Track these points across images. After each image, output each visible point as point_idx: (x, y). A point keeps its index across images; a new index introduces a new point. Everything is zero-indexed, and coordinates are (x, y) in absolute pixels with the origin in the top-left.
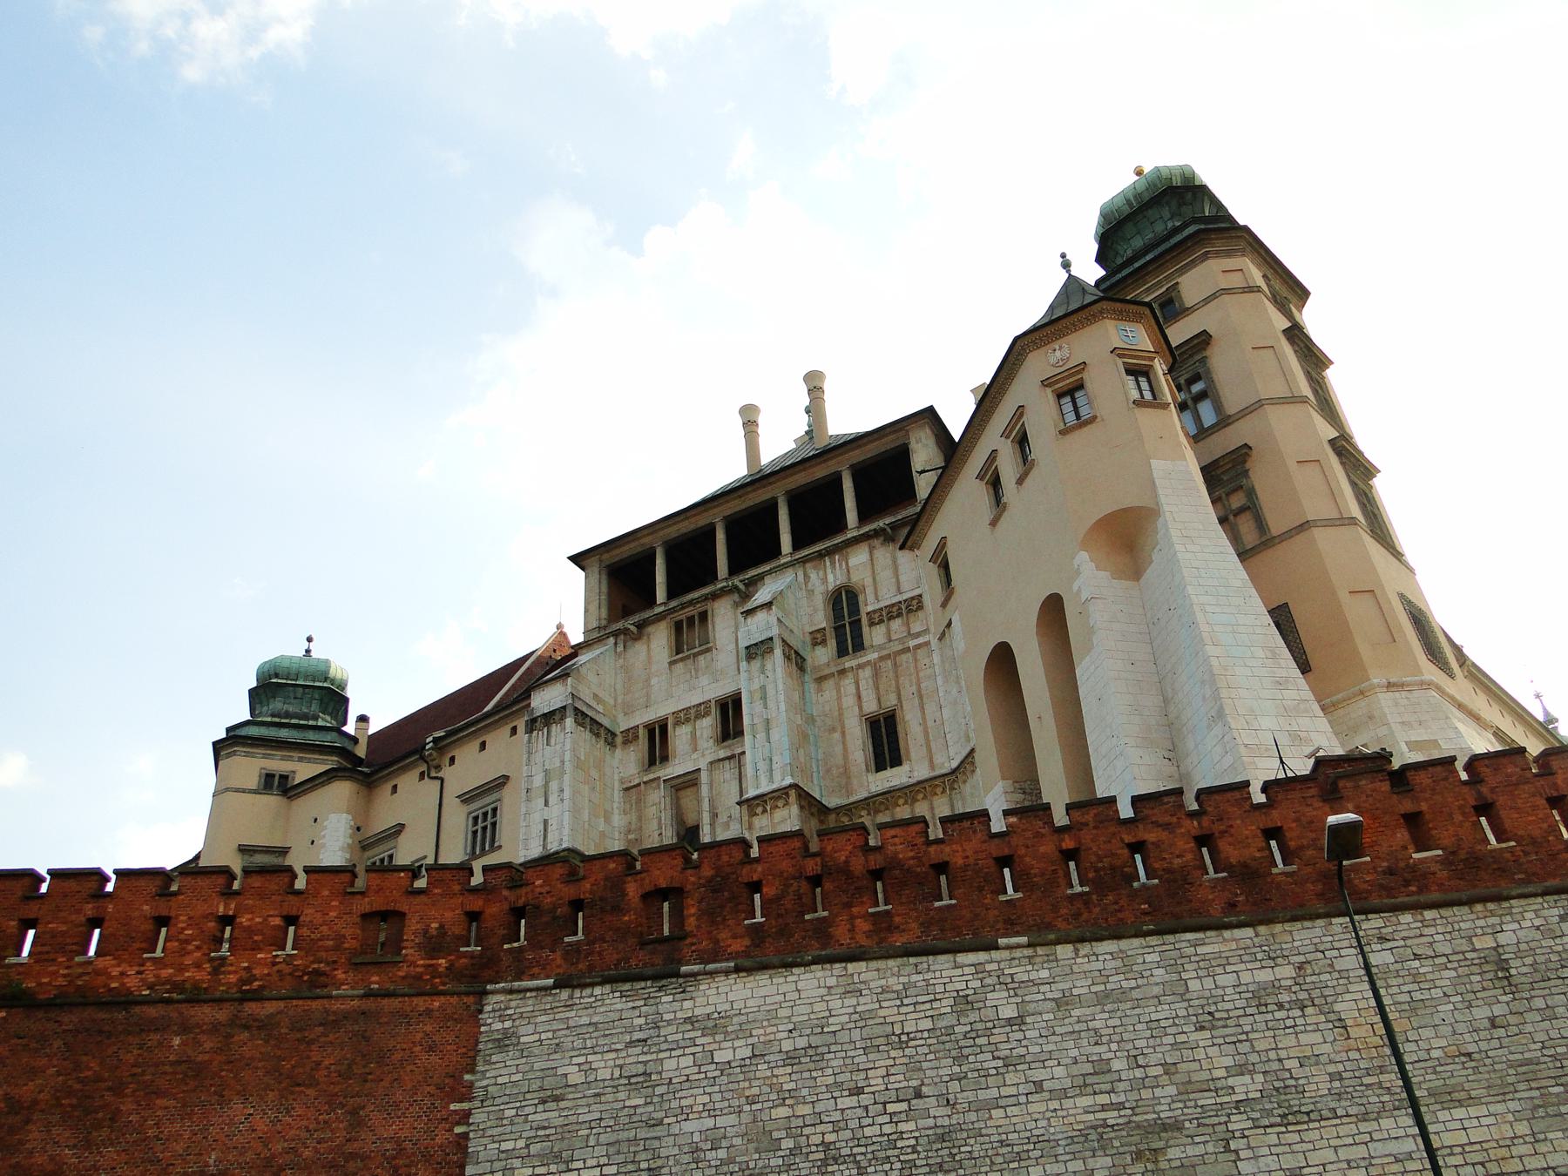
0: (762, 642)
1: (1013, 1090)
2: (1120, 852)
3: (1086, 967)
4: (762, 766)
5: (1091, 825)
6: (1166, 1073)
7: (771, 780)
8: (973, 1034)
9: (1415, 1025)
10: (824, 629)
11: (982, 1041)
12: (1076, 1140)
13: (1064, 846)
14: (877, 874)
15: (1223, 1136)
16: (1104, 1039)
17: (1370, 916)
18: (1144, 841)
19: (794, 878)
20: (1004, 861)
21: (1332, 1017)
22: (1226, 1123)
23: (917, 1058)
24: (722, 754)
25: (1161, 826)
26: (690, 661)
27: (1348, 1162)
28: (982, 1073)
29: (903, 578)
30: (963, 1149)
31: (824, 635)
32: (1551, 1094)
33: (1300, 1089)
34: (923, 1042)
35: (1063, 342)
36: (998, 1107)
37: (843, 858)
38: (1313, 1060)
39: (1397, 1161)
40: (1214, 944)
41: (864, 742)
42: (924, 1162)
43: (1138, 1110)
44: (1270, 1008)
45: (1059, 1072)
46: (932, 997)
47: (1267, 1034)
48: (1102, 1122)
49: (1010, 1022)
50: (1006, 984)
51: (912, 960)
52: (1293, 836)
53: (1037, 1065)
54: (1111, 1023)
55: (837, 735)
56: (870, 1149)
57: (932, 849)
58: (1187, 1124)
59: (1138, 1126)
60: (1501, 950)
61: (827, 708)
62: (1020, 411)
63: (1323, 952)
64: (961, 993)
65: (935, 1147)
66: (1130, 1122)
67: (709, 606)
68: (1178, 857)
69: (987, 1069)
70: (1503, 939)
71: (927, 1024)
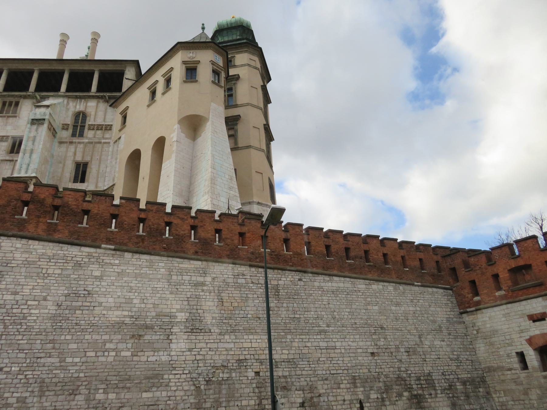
0: (40, 119)
1: (88, 304)
2: (161, 224)
3: (135, 263)
4: (24, 167)
5: (154, 211)
6: (154, 307)
7: (26, 172)
8: (79, 279)
9: (246, 305)
10: (69, 125)
11: (82, 283)
12: (109, 327)
13: (141, 216)
14: (56, 208)
15: (168, 333)
16: (133, 291)
17: (242, 266)
18: (172, 222)
19: (16, 200)
20: (114, 216)
21: (220, 297)
22: (170, 329)
23: (49, 284)
24: (8, 158)
25: (180, 218)
26: (5, 119)
27: (210, 348)
28: (77, 295)
29: (107, 117)
30: (58, 324)
31: (68, 127)
32: (280, 335)
33: (201, 321)
34: (54, 278)
35: (195, 51)
36: (80, 310)
37: (43, 197)
38: (208, 311)
39: (226, 350)
40: (186, 264)
41: (71, 171)
42: (38, 327)
43: (138, 319)
44: (199, 290)
45: (111, 300)
46: (65, 261)
47: (195, 299)
48: (122, 322)
49: (96, 277)
50: (99, 262)
51: (61, 245)
52: (225, 233)
53: (102, 296)
54: (138, 285)
55: (61, 165)
56: (13, 318)
57: (85, 204)
58: (156, 327)
59: (136, 325)
60: (278, 286)
61: (60, 154)
62: (172, 69)
63: (223, 275)
64: (78, 262)
65: (45, 321)
66: (134, 323)
67: (22, 100)
68: (183, 231)
69: (80, 294)
70: (280, 282)
71: (59, 271)
